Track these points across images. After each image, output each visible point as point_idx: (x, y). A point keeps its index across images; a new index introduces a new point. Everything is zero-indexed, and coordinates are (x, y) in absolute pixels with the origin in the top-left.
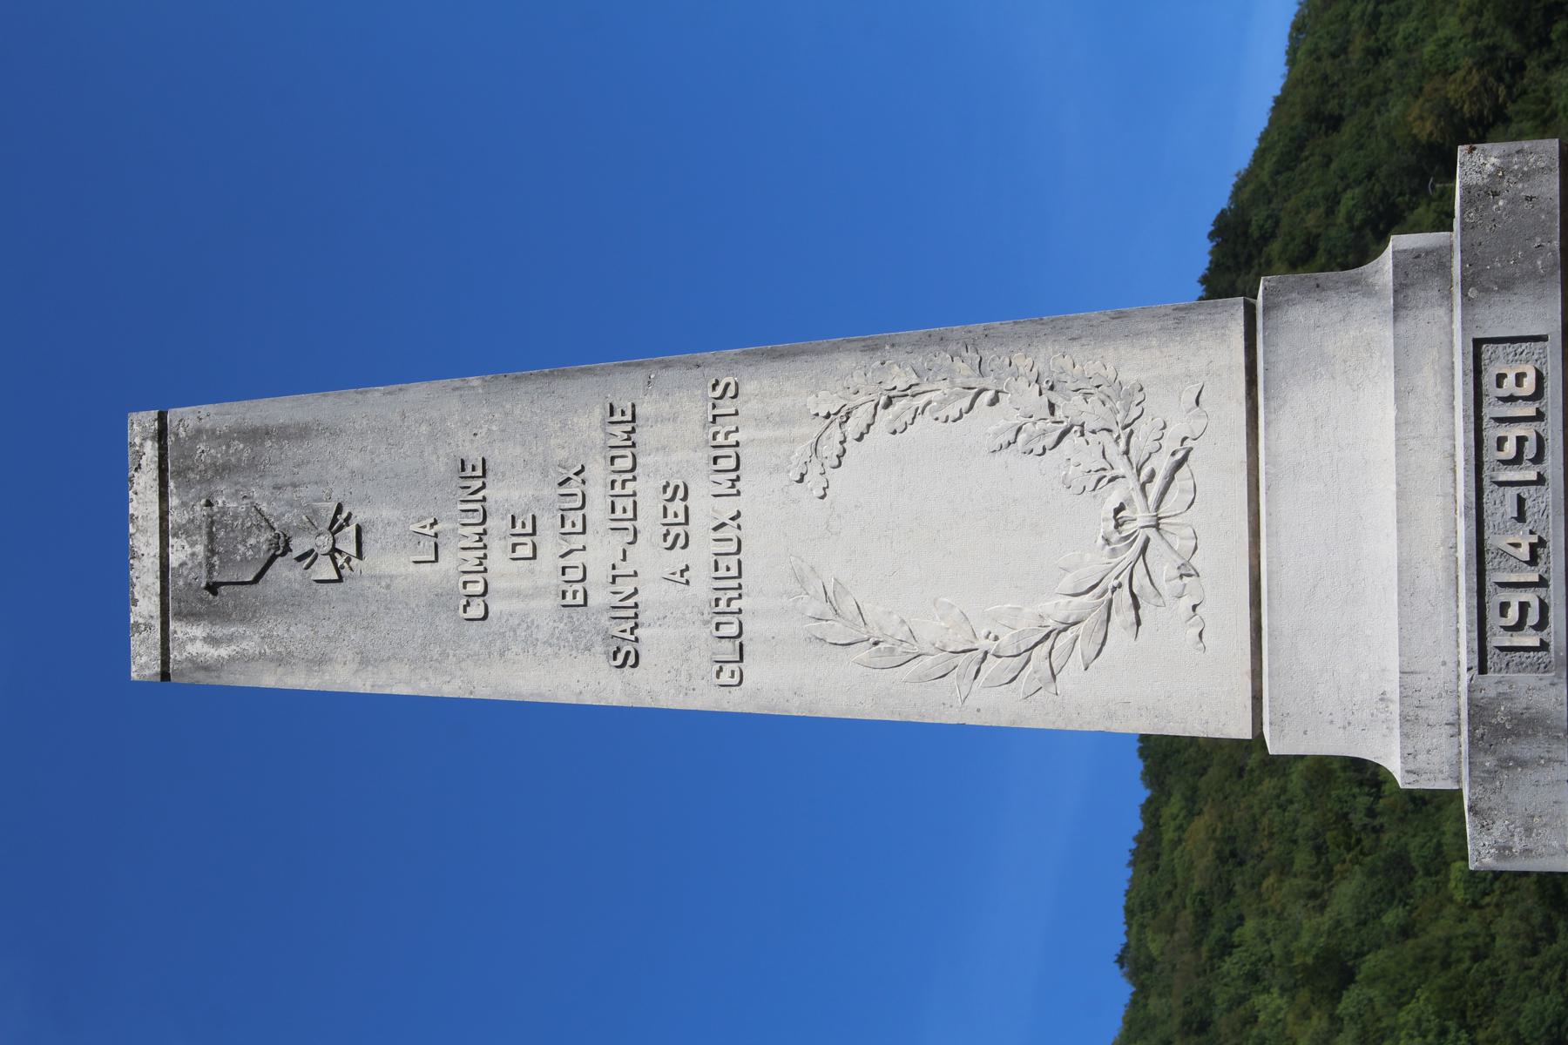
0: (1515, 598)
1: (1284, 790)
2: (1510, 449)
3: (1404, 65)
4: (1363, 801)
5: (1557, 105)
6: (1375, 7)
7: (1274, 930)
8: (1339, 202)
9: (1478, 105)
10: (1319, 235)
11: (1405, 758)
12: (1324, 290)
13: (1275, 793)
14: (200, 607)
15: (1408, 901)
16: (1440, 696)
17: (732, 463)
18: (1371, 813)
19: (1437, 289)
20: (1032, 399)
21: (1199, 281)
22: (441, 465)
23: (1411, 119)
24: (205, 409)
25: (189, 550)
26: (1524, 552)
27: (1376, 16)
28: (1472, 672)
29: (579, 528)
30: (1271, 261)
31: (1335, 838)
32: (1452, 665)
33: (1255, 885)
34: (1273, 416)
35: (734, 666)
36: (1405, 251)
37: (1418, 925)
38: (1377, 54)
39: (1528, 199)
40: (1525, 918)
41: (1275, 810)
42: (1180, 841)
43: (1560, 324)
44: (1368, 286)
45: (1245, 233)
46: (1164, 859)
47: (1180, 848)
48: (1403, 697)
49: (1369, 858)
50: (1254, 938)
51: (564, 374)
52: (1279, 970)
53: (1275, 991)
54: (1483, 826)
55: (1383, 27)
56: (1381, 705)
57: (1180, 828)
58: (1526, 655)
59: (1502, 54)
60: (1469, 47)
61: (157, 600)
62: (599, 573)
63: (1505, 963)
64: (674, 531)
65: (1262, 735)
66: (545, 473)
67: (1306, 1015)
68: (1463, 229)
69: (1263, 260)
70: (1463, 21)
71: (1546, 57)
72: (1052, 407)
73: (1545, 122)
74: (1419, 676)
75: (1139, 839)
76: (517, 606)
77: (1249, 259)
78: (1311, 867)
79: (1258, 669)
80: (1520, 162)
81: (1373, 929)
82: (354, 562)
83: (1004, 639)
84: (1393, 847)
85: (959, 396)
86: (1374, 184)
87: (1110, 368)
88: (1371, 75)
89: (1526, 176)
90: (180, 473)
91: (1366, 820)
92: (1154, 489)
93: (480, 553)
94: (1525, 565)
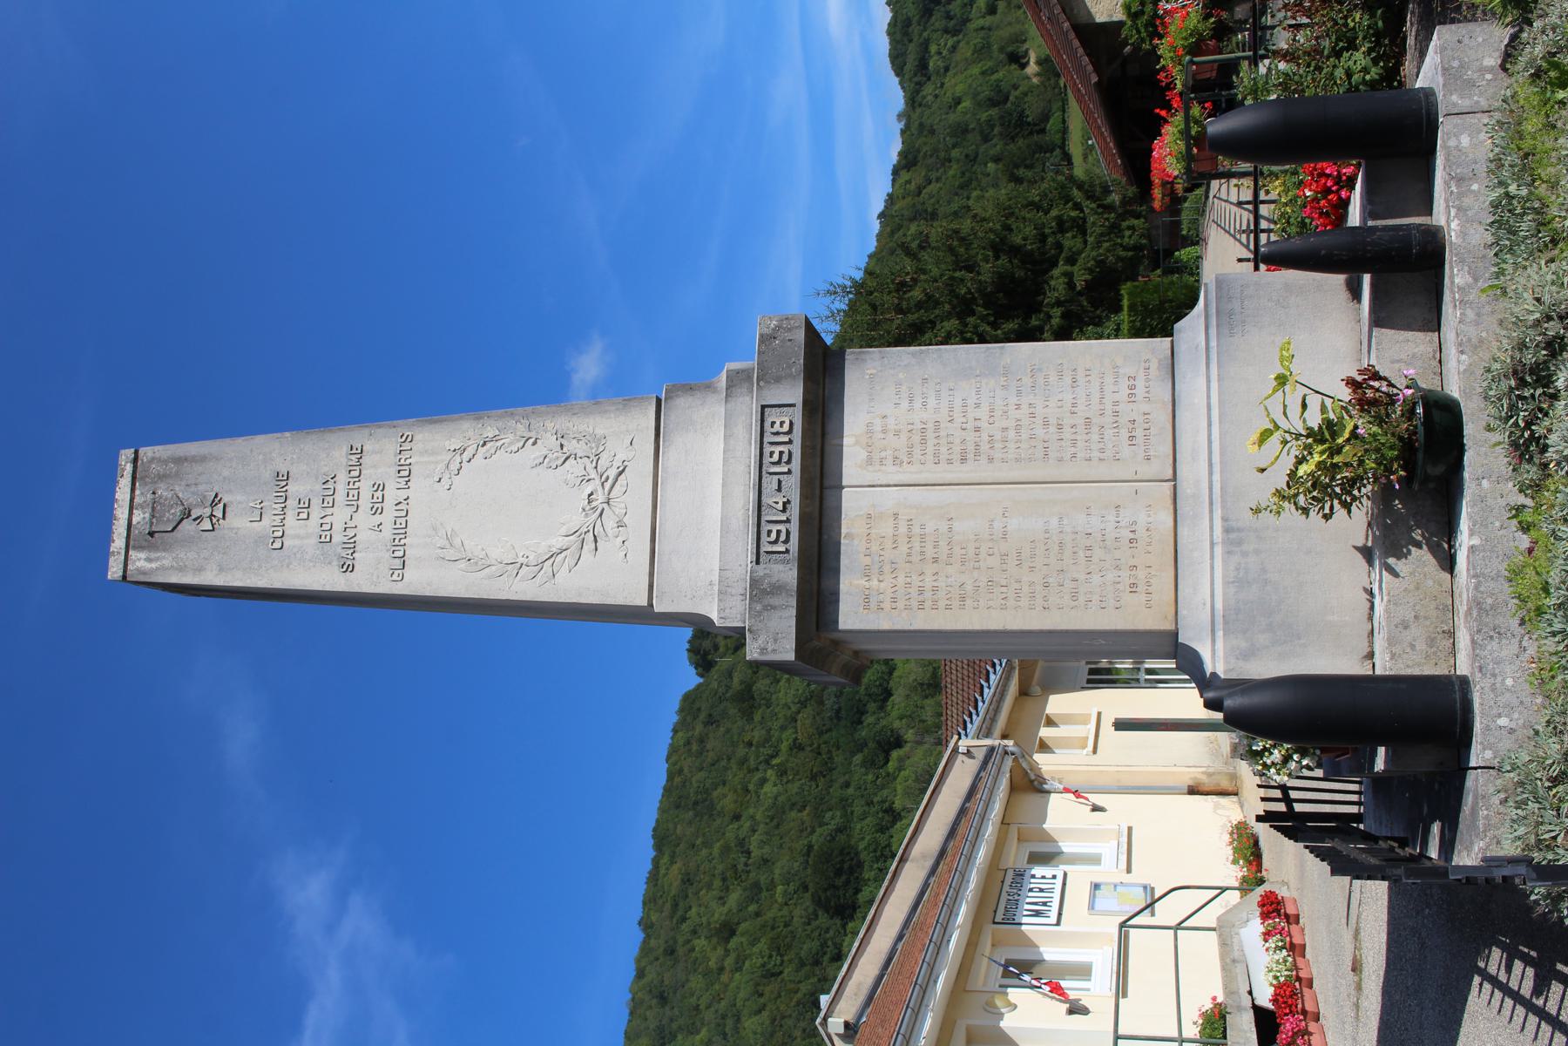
0: (775, 528)
1: (711, 854)
2: (776, 457)
4: (743, 860)
11: (719, 613)
14: (144, 544)
17: (407, 473)
18: (746, 865)
20: (552, 442)
22: (268, 475)
24: (157, 448)
25: (142, 516)
26: (780, 506)
29: (331, 505)
32: (744, 566)
33: (697, 893)
35: (400, 571)
39: (790, 340)
40: (805, 910)
46: (659, 882)
51: (331, 431)
53: (703, 938)
61: (124, 540)
62: (338, 527)
64: (376, 505)
66: (317, 478)
67: (715, 948)
72: (562, 446)
75: (650, 873)
76: (297, 542)
82: (221, 521)
83: (531, 558)
85: (518, 441)
87: (591, 428)
89: (790, 330)
90: (142, 478)
92: (608, 486)
93: (282, 517)
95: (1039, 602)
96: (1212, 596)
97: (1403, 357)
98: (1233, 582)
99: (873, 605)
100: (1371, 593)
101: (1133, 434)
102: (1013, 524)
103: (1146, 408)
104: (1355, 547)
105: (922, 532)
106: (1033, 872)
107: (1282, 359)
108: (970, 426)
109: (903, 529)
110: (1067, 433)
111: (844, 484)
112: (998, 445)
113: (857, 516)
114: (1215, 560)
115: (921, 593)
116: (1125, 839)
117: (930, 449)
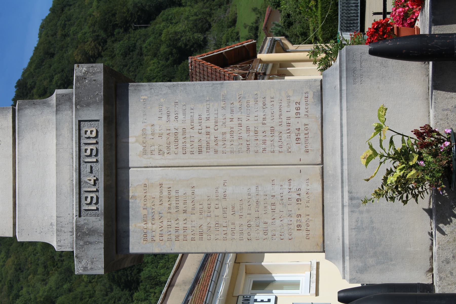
0: (89, 195)
1: (35, 250)
2: (88, 152)
3: (73, 39)
5: (116, 53)
6: (64, 22)
7: (32, 291)
8: (53, 78)
9: (94, 52)
10: (47, 88)
12: (36, 105)
13: (32, 250)
15: (71, 281)
16: (68, 224)
19: (68, 105)
21: (12, 100)
23: (74, 55)
26: (92, 182)
27: (65, 25)
28: (77, 217)
30: (33, 95)
31: (50, 263)
32: (71, 215)
33: (26, 278)
34: (20, 142)
36: (59, 94)
37: (74, 288)
38: (65, 36)
39: (94, 80)
41: (32, 256)
42: (4, 265)
43: (103, 117)
44: (48, 104)
45: (26, 86)
47: (4, 267)
48: (57, 224)
49: (60, 269)
50: (26, 293)
52: (33, 302)
54: (79, 262)
55: (67, 28)
56: (51, 227)
57: (4, 261)
58: (92, 212)
59: (101, 38)
60: (91, 35)
63: (98, 299)
65: (16, 236)
68: (76, 88)
69: (31, 94)
70: (89, 27)
71: (113, 39)
73: (112, 58)
74: (62, 218)
77: (27, 94)
78: (43, 272)
79: (15, 216)
80: (92, 70)
81: (61, 290)
84: (67, 266)
86: (64, 73)
88: (63, 42)
89: (94, 74)
91: (59, 258)
94: (92, 186)
95: (245, 236)
96: (343, 236)
97: (449, 107)
98: (354, 229)
99: (149, 238)
100: (431, 234)
101: (298, 137)
102: (230, 190)
103: (305, 121)
104: (424, 209)
105: (177, 195)
106: (256, 297)
107: (379, 116)
108: (203, 131)
109: (165, 193)
110: (260, 137)
111: (130, 166)
112: (220, 143)
113: (137, 185)
114: (345, 215)
115: (177, 231)
116: (314, 272)
117: (180, 145)
